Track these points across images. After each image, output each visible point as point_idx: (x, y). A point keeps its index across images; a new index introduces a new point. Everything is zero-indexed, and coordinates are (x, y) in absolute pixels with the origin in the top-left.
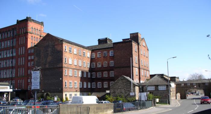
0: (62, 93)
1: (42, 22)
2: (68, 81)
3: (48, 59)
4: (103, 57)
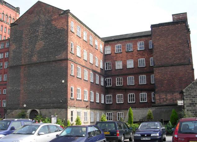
0: (66, 108)
1: (17, 8)
2: (75, 87)
3: (36, 46)
4: (127, 52)
